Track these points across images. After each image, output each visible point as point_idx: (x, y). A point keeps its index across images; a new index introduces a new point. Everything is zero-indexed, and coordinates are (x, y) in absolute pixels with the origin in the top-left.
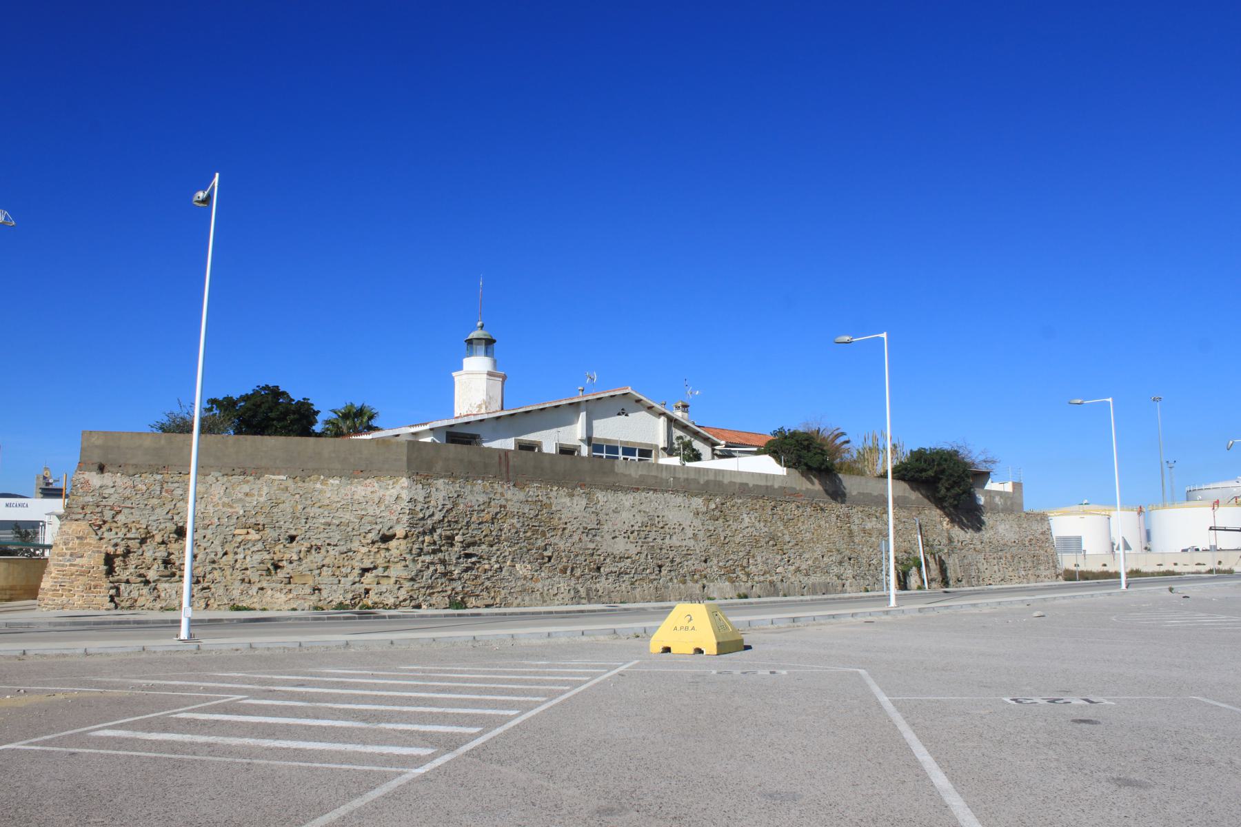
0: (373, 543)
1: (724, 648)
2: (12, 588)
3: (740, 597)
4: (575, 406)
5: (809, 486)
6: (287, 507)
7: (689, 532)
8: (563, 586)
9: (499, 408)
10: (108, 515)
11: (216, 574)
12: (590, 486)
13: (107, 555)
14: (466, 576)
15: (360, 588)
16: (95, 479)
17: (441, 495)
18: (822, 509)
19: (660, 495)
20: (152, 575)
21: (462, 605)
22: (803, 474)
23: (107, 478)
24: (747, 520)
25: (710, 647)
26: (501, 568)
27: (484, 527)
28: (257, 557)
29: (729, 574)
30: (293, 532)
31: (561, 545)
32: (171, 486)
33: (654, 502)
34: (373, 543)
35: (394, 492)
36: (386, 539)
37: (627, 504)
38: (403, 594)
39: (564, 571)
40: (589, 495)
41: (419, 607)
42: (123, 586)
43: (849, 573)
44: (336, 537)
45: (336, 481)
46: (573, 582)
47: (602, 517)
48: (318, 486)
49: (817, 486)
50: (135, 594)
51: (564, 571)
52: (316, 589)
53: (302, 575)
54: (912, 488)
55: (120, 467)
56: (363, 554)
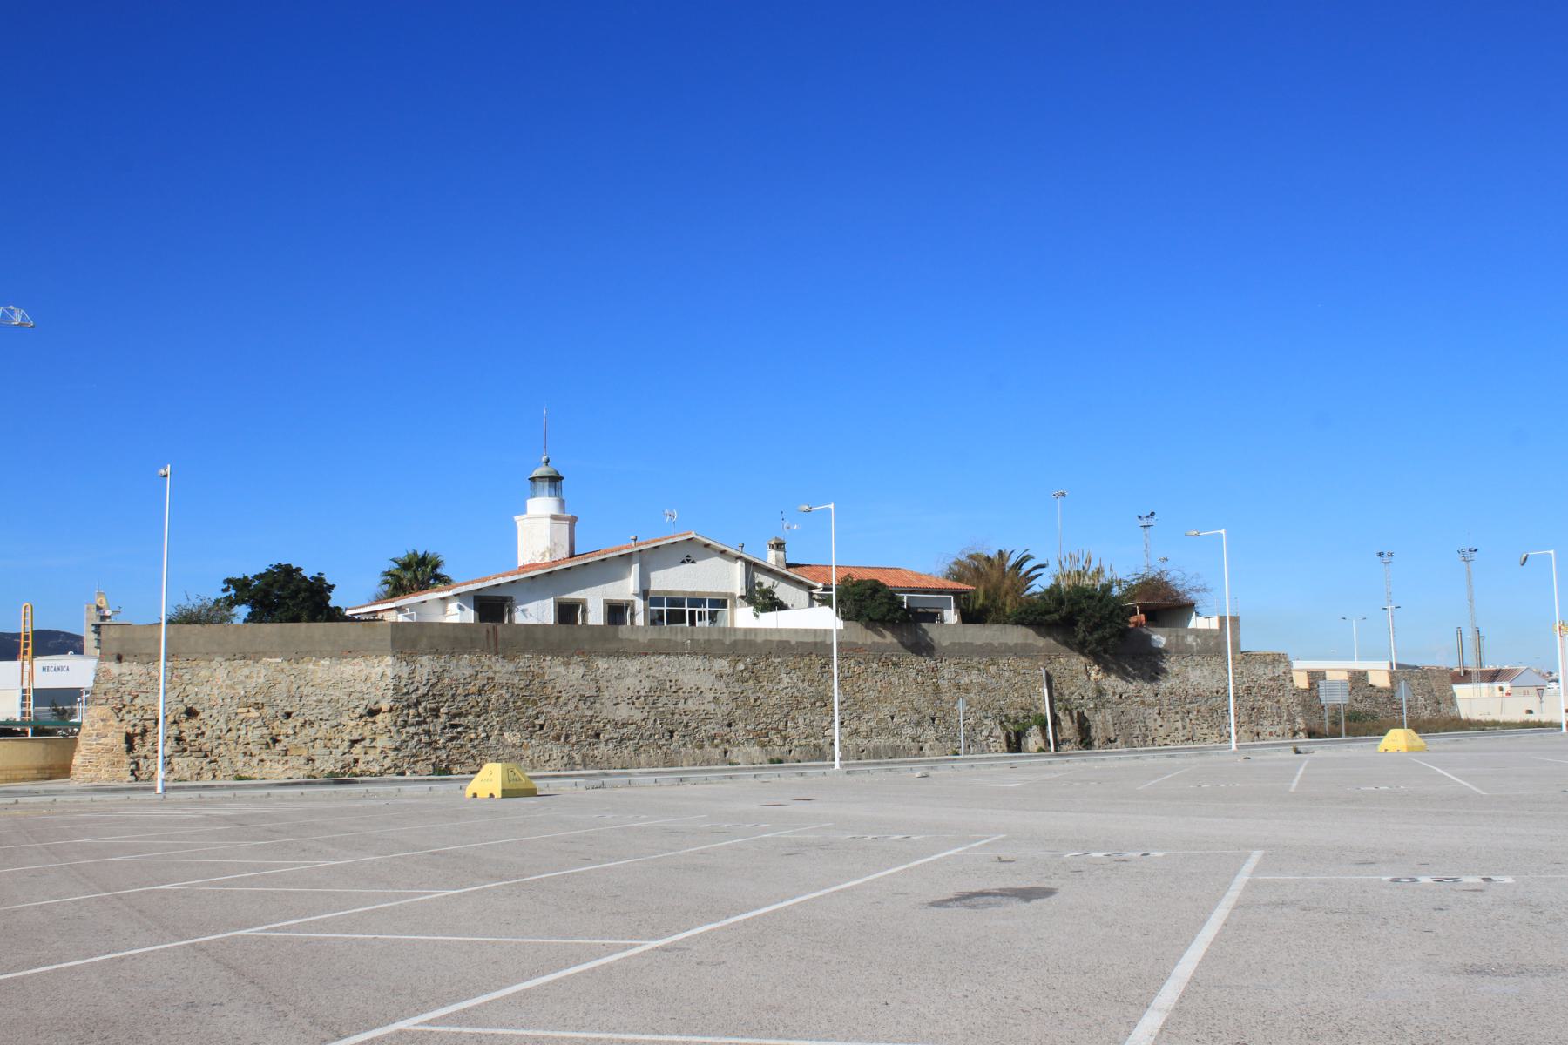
0: (361, 717)
1: (506, 793)
2: (50, 767)
3: (772, 761)
4: (627, 558)
5: (877, 639)
6: (283, 687)
7: (709, 696)
8: (556, 753)
9: (566, 555)
10: (127, 699)
11: (222, 749)
12: (590, 654)
13: (128, 735)
14: (450, 745)
15: (349, 758)
17: (425, 671)
18: (895, 664)
19: (673, 659)
21: (448, 771)
22: (867, 627)
23: (125, 667)
24: (786, 680)
25: (498, 794)
26: (488, 737)
27: (470, 698)
28: (258, 732)
29: (760, 738)
30: (288, 710)
31: (555, 713)
32: (181, 672)
33: (664, 667)
34: (361, 717)
35: (379, 670)
36: (373, 713)
37: (633, 670)
38: (388, 763)
39: (558, 738)
40: (587, 665)
41: (403, 774)
42: (141, 762)
43: (931, 734)
44: (327, 712)
45: (326, 662)
46: (567, 749)
47: (602, 684)
48: (311, 667)
49: (889, 638)
51: (558, 738)
52: (310, 760)
53: (297, 748)
54: (1039, 634)
55: (135, 656)
56: (352, 728)
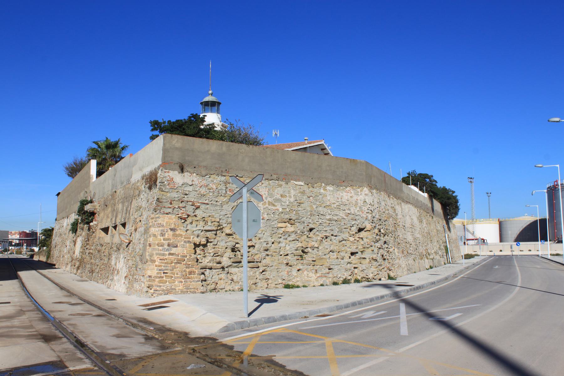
16: (178, 178)
20: (226, 261)
30: (311, 226)
50: (216, 278)
55: (196, 168)
